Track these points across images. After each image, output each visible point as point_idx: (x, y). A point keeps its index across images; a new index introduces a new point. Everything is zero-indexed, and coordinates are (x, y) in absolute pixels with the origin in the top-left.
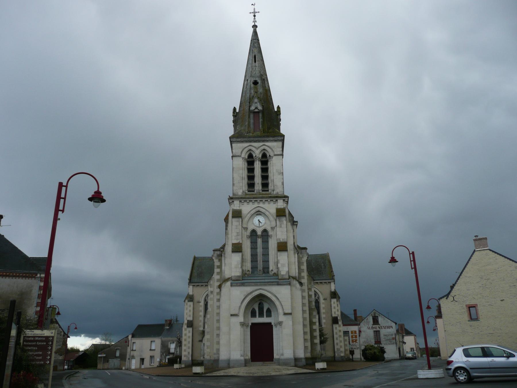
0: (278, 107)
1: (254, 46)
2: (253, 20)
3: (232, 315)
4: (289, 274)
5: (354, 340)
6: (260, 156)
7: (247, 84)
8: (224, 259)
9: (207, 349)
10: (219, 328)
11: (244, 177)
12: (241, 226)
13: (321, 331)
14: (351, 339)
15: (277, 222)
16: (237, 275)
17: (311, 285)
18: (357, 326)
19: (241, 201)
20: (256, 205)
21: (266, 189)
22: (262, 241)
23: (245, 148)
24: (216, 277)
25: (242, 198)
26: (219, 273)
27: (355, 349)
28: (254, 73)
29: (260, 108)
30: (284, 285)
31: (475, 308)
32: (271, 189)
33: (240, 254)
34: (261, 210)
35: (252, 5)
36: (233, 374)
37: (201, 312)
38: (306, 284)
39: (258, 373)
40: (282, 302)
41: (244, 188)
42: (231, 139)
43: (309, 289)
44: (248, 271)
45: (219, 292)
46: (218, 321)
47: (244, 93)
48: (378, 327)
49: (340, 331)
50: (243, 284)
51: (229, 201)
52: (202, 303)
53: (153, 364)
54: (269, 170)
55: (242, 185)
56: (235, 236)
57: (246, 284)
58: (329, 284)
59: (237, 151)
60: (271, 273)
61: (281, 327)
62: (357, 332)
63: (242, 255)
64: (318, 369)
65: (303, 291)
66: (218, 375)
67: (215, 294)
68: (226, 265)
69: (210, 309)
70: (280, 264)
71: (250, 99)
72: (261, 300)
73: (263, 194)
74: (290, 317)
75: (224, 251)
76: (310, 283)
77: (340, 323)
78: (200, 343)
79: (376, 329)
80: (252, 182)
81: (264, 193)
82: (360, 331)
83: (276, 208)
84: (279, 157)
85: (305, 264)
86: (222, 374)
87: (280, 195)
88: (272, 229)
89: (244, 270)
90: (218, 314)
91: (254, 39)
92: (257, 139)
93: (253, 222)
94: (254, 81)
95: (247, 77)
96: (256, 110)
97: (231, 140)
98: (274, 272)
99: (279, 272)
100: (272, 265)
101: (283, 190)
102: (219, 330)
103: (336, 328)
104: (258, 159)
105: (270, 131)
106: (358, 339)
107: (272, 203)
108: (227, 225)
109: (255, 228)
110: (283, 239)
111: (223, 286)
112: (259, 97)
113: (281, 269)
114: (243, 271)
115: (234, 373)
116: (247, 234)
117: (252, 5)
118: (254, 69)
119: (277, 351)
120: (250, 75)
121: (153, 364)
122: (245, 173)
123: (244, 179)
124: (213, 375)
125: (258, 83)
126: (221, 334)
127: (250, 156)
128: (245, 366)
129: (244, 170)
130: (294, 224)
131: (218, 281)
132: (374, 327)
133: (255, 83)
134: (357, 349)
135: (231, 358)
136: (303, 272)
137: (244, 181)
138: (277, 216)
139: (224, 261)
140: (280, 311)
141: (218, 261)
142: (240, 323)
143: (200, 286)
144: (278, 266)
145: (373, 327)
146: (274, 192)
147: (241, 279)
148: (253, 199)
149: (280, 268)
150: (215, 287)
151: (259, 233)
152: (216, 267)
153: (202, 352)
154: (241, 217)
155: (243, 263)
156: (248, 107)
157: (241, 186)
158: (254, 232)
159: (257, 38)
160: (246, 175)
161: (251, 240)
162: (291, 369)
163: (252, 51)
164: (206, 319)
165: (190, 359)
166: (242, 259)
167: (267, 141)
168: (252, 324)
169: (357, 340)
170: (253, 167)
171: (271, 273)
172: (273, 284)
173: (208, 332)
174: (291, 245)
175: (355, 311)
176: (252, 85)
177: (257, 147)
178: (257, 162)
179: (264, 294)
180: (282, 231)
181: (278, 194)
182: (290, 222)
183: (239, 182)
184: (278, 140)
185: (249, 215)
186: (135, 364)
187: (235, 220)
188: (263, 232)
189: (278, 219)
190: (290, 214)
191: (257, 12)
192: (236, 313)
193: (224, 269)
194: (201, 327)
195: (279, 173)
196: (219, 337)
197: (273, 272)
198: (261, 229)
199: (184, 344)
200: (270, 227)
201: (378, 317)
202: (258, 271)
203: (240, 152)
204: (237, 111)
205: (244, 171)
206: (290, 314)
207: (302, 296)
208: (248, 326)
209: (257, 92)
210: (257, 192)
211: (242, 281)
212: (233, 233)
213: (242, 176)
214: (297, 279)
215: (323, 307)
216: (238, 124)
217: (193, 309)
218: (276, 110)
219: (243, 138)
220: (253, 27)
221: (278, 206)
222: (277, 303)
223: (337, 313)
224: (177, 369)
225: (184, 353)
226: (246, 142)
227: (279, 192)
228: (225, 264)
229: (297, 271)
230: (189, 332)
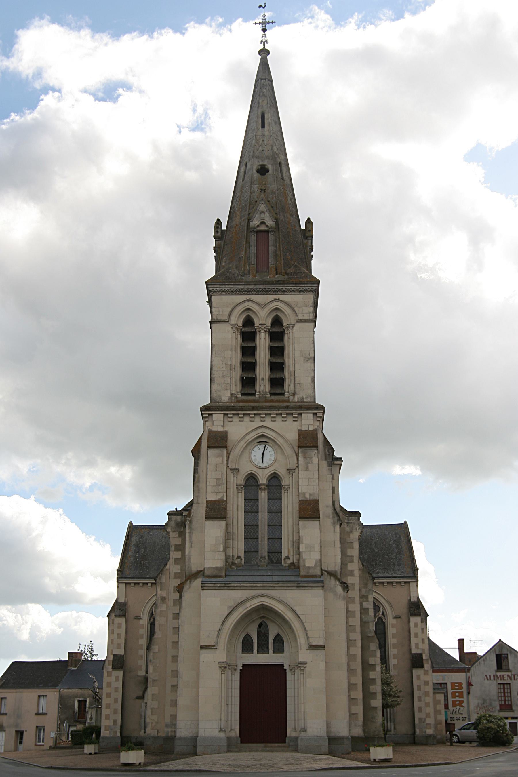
0: (309, 222)
1: (261, 94)
2: (261, 39)
3: (202, 647)
4: (321, 565)
5: (458, 702)
6: (269, 322)
7: (245, 172)
8: (190, 533)
9: (152, 714)
10: (175, 674)
11: (235, 366)
12: (226, 465)
13: (385, 683)
14: (450, 699)
15: (300, 459)
16: (214, 566)
17: (367, 589)
18: (464, 674)
19: (227, 414)
20: (257, 422)
21: (279, 391)
22: (268, 496)
23: (237, 305)
24: (172, 568)
25: (228, 408)
26: (181, 561)
27: (459, 719)
28: (261, 149)
29: (270, 223)
30: (311, 587)
31: (13, 749)
32: (288, 392)
33: (223, 523)
34: (268, 433)
35: (260, 6)
36: (203, 768)
37: (142, 638)
38: (357, 588)
39: (253, 765)
40: (306, 622)
41: (233, 387)
42: (209, 286)
43: (364, 597)
44: (239, 557)
45: (178, 600)
46: (175, 658)
47: (238, 190)
48: (508, 675)
49: (426, 683)
50: (228, 585)
51: (202, 414)
52: (144, 621)
53: (41, 743)
54: (286, 352)
55: (229, 382)
56: (214, 486)
57: (233, 585)
58: (407, 585)
59: (223, 313)
60: (285, 563)
61: (303, 674)
62: (464, 686)
63: (227, 525)
64: (375, 760)
65: (349, 601)
66: (171, 768)
67: (171, 603)
68: (193, 545)
69: (158, 635)
70: (304, 545)
71: (250, 203)
72: (263, 617)
73: (272, 401)
74: (320, 653)
75: (190, 517)
76: (366, 585)
77: (427, 666)
78: (140, 701)
79: (503, 679)
80: (250, 376)
81: (273, 397)
82: (469, 684)
83: (299, 430)
84: (307, 324)
85: (356, 545)
86: (180, 767)
87: (308, 404)
88: (289, 472)
89: (229, 555)
90: (176, 644)
91: (261, 79)
92: (262, 287)
93: (250, 457)
94: (259, 165)
95: (245, 158)
96: (263, 228)
97: (210, 289)
98: (291, 561)
99: (301, 561)
100: (286, 547)
101: (313, 395)
102: (177, 677)
103: (419, 677)
104: (263, 328)
105: (292, 270)
106: (465, 699)
107: (290, 419)
108: (198, 462)
109: (254, 470)
110: (310, 495)
111: (186, 587)
112: (269, 200)
113: (304, 556)
114: (227, 557)
115: (204, 764)
116: (239, 483)
117: (260, 6)
118: (261, 142)
119: (293, 722)
120: (251, 153)
121: (43, 744)
122: (237, 357)
123: (235, 368)
124: (162, 768)
125: (268, 171)
126: (180, 685)
127: (249, 322)
128: (229, 751)
129: (235, 351)
130: (336, 463)
131: (176, 576)
132: (499, 676)
133: (263, 171)
134: (463, 720)
135: (200, 734)
136: (352, 561)
137: (233, 373)
138: (299, 447)
139: (190, 537)
140: (302, 640)
141: (177, 536)
142: (220, 663)
143: (141, 585)
144: (299, 549)
145: (497, 676)
146: (294, 397)
147: (223, 574)
148: (252, 411)
149: (303, 554)
150: (172, 589)
151: (263, 480)
152: (173, 548)
153: (143, 720)
154: (226, 447)
155: (228, 541)
156: (247, 221)
157: (227, 384)
158: (251, 478)
159: (267, 77)
160: (239, 361)
161: (245, 493)
162: (320, 760)
163: (256, 104)
164: (151, 654)
165: (118, 734)
166: (227, 532)
167: (284, 292)
168: (244, 666)
169: (463, 702)
170: (253, 345)
171: (285, 563)
172: (289, 585)
173: (154, 681)
174: (327, 506)
175: (461, 642)
176: (256, 175)
177: (262, 304)
178: (263, 334)
179: (270, 606)
180: (309, 478)
181: (304, 402)
182: (326, 459)
183: (223, 376)
184: (306, 290)
185: (242, 444)
186: (5, 742)
187: (212, 452)
188: (271, 478)
189: (302, 452)
190: (326, 442)
191: (269, 23)
192: (212, 644)
193: (189, 552)
194: (141, 670)
195: (307, 359)
196: (176, 691)
197: (289, 562)
198: (268, 472)
199: (108, 683)
200: (286, 470)
201: (507, 654)
202: (259, 558)
203: (227, 313)
204: (224, 228)
205: (234, 352)
206: (323, 647)
207: (348, 611)
208: (235, 670)
209: (265, 190)
210: (259, 397)
211: (226, 579)
212: (208, 480)
213: (229, 363)
214: (339, 577)
215: (393, 634)
216: (224, 254)
217: (126, 633)
218: (303, 227)
219: (233, 285)
220: (259, 54)
221: (302, 426)
222: (295, 624)
223: (421, 646)
224: (91, 754)
225: (104, 723)
226: (240, 292)
227: (305, 397)
228: (191, 543)
229: (339, 561)
230: (117, 679)
